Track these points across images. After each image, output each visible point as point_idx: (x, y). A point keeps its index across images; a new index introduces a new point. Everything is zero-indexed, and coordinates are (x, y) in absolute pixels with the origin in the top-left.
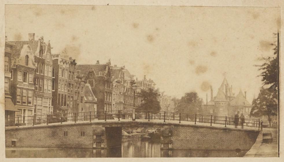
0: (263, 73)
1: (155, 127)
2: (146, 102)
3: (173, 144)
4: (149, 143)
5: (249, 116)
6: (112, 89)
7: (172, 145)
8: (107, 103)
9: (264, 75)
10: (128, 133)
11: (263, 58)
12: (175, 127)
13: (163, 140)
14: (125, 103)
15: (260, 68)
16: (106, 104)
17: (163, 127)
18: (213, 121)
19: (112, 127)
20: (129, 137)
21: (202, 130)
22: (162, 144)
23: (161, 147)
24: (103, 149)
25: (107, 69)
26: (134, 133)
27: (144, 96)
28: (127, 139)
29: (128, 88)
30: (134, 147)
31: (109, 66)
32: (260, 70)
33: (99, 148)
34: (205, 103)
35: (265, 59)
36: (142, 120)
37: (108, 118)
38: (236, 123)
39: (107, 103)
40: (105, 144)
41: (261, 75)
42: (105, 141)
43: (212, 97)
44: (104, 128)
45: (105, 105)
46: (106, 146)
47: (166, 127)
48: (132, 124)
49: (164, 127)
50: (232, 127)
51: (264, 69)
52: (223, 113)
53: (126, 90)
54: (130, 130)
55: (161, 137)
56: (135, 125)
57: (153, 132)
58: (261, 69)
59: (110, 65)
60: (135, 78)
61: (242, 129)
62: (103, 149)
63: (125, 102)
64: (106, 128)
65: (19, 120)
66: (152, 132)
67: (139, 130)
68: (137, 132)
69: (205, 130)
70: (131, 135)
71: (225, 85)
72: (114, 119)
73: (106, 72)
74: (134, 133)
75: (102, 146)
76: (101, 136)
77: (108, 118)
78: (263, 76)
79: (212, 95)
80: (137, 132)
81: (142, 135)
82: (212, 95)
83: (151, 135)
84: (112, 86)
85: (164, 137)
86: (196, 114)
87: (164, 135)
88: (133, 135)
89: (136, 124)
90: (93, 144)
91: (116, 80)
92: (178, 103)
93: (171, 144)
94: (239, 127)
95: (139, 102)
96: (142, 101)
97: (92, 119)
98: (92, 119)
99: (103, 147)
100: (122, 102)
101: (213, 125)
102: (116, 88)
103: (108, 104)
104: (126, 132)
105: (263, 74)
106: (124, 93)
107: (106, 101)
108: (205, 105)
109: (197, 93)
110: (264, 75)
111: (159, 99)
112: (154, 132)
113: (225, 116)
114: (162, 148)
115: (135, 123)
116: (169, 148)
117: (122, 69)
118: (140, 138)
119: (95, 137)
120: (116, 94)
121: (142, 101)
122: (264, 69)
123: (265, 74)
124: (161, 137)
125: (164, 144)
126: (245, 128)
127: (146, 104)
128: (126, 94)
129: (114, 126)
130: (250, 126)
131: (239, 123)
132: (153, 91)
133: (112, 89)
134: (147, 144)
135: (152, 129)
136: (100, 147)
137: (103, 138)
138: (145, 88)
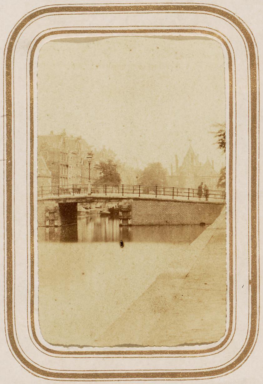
0: (219, 140)
1: (113, 202)
2: (105, 175)
3: (133, 219)
4: (109, 219)
5: (217, 187)
6: (68, 161)
7: (132, 220)
8: (65, 177)
9: (220, 143)
10: (86, 208)
11: (219, 124)
12: (135, 201)
13: (121, 215)
14: (83, 176)
15: (215, 135)
16: (61, 177)
17: (121, 202)
18: (175, 194)
19: (67, 203)
20: (87, 213)
21: (162, 203)
22: (121, 220)
23: (120, 223)
24: (56, 226)
25: (62, 140)
26: (93, 208)
27: (103, 168)
28: (84, 215)
29: (85, 159)
30: (93, 225)
31: (64, 136)
32: (216, 136)
33: (52, 227)
34: (170, 175)
35: (221, 125)
36: (102, 195)
37: (67, 193)
38: (200, 195)
39: (65, 177)
40: (58, 222)
41: (218, 142)
42: (59, 218)
43: (177, 168)
44: (57, 205)
45: (60, 179)
46: (60, 224)
47: (125, 201)
48: (88, 199)
49: (122, 201)
50: (196, 199)
51: (220, 136)
52: (192, 184)
53: (84, 162)
54: (88, 206)
55: (120, 212)
56: (91, 200)
57: (113, 207)
58: (217, 136)
59: (65, 135)
60: (92, 149)
61: (206, 201)
62: (56, 226)
63: (82, 175)
64: (60, 204)
65: (192, 192)
66: (112, 207)
67: (99, 205)
68: (96, 208)
69: (166, 204)
70: (89, 210)
71: (191, 154)
72: (70, 194)
73: (61, 143)
74: (93, 208)
75: (56, 224)
76: (54, 213)
77: (67, 193)
78: (219, 144)
79: (177, 165)
80: (96, 208)
81: (102, 211)
82: (177, 165)
83: (111, 210)
84: (68, 158)
85: (123, 212)
86: (157, 187)
87: (122, 209)
88: (91, 211)
89: (92, 199)
90: (45, 222)
91: (72, 151)
92: (141, 175)
93: (131, 220)
94: (203, 199)
95: (98, 174)
96: (100, 173)
97: (108, 192)
98: (108, 192)
99: (131, 223)
100: (79, 175)
101: (176, 198)
102: (72, 160)
103: (64, 178)
104: (84, 208)
105: (219, 142)
106: (81, 165)
107: (61, 174)
108: (171, 177)
109: (160, 163)
110: (220, 143)
111: (119, 171)
112: (115, 207)
113: (188, 188)
114: (121, 224)
115: (90, 198)
116: (128, 224)
117: (78, 139)
118: (99, 214)
119: (47, 214)
120: (73, 167)
121: (100, 173)
122: (220, 136)
123: (221, 141)
124: (120, 212)
125: (123, 219)
126: (210, 200)
127: (104, 177)
128: (84, 166)
129: (68, 201)
130: (219, 198)
131: (203, 194)
132: (112, 162)
133: (68, 161)
134: (107, 219)
135: (113, 204)
136: (53, 225)
137: (57, 215)
138: (104, 160)
